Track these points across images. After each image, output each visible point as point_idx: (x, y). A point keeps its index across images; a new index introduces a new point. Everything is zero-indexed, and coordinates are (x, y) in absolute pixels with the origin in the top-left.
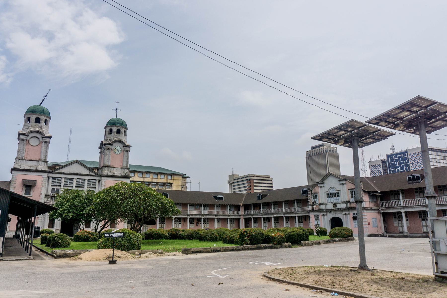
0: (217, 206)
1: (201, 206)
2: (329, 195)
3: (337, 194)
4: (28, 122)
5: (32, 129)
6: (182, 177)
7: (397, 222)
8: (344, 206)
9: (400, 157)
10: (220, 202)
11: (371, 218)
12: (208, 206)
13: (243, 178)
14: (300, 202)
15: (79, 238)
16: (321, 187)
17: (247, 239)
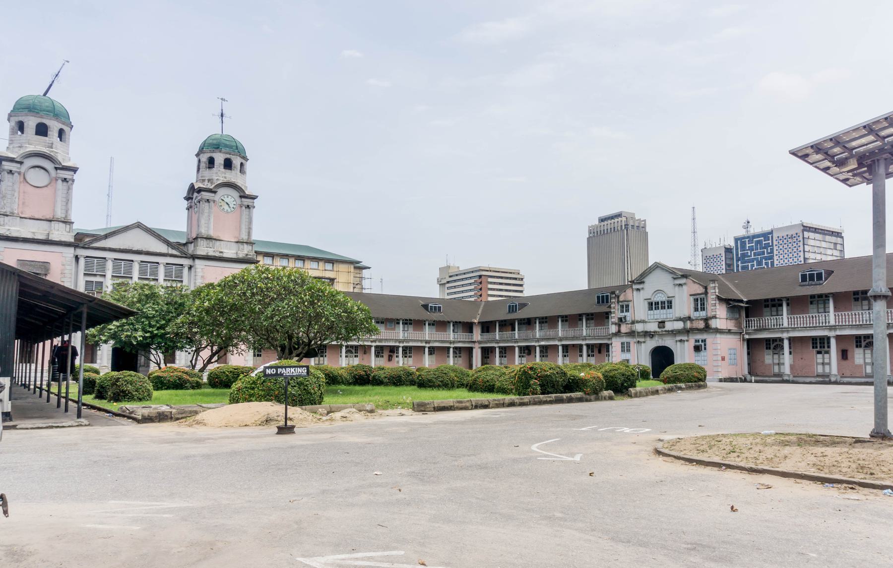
0: (429, 324)
1: (398, 323)
2: (653, 305)
3: (669, 304)
4: (19, 133)
5: (31, 148)
6: (355, 268)
7: (770, 357)
8: (679, 325)
9: (759, 242)
10: (436, 316)
11: (724, 351)
12: (411, 324)
13: (468, 273)
14: (592, 319)
15: (162, 383)
16: (638, 290)
17: (535, 384)
